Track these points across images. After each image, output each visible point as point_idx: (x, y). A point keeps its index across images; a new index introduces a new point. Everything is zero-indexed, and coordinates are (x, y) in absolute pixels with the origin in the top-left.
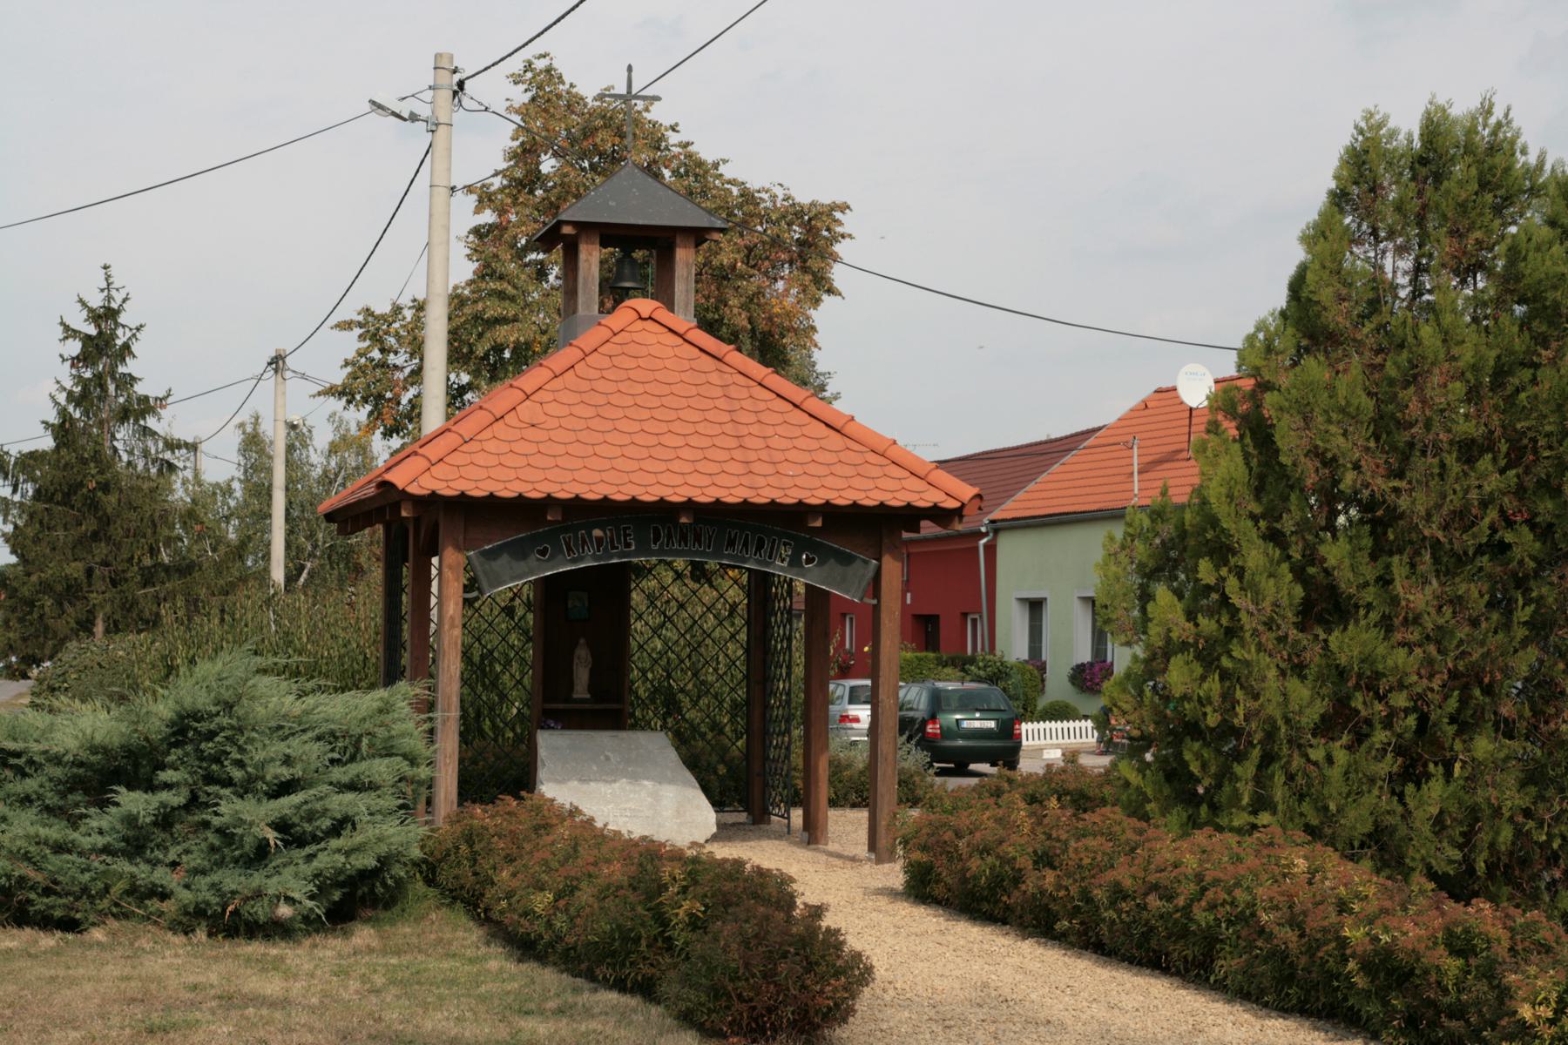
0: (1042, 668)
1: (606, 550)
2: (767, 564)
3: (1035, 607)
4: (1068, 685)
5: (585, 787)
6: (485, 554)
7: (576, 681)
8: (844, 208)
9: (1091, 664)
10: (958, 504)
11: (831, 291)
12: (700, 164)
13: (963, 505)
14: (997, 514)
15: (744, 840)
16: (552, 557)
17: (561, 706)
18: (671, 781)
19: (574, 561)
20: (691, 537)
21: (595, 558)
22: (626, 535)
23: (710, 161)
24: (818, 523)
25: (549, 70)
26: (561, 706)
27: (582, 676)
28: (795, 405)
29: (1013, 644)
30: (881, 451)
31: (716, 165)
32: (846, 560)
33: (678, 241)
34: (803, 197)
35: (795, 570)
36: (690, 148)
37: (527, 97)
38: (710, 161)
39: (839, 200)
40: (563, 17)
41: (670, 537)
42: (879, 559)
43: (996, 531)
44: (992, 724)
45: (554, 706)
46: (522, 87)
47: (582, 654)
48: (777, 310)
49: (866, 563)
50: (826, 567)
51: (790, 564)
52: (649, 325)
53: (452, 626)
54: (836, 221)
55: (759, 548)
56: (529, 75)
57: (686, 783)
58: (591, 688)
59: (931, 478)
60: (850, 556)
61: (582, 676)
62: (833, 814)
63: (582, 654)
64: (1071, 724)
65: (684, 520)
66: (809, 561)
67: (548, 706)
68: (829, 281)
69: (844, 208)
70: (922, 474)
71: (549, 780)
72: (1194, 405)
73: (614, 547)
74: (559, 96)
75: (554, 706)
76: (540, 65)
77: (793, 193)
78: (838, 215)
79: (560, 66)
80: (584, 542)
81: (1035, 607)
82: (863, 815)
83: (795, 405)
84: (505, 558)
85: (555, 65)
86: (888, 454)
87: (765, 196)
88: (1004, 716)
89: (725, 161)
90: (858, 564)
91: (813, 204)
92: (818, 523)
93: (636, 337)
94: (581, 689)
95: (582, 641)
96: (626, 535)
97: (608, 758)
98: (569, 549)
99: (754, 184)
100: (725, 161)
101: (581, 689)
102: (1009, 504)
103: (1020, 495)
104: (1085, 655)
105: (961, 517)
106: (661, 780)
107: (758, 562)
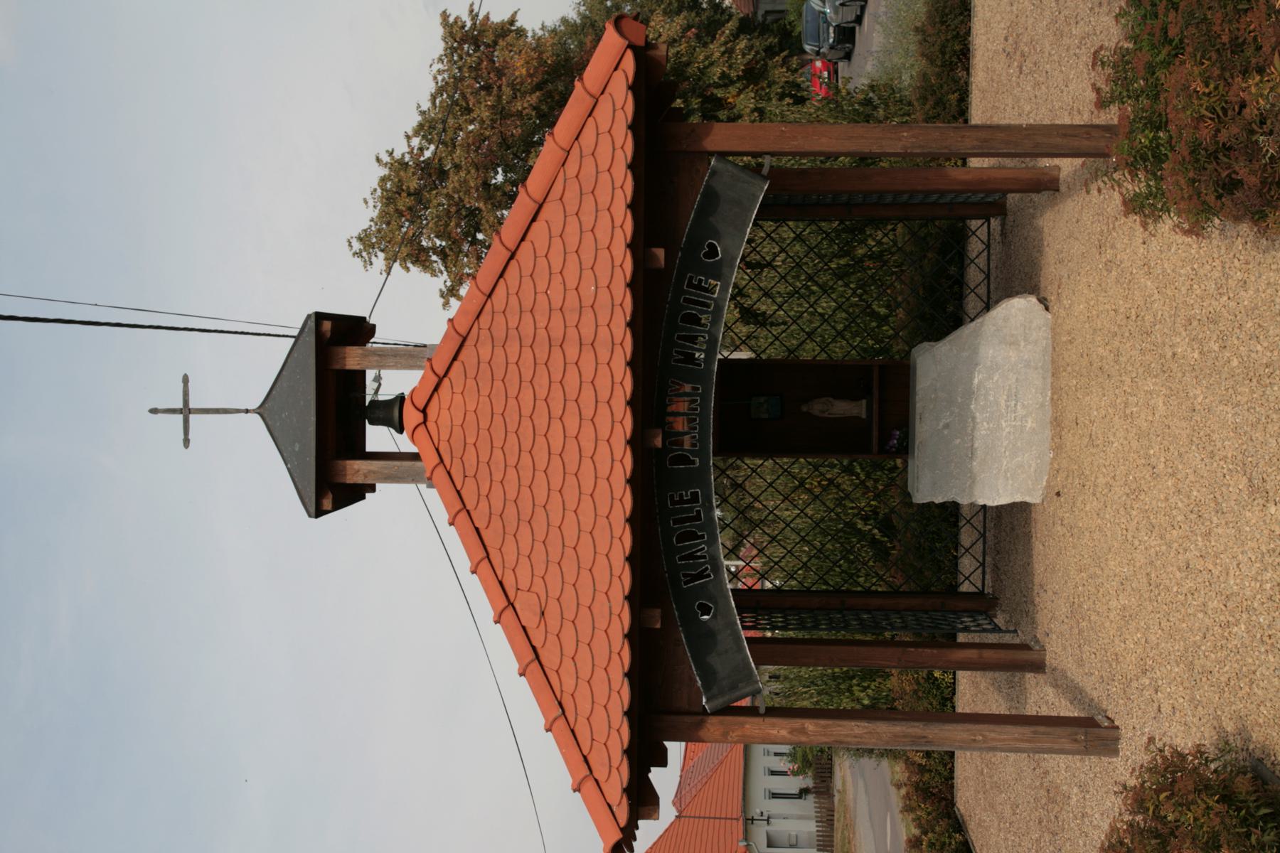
1: (701, 528)
5: (979, 453)
6: (707, 686)
8: (445, 16)
10: (629, 54)
11: (512, 21)
12: (421, 126)
13: (629, 46)
15: (1040, 252)
17: (875, 433)
18: (975, 350)
22: (682, 501)
23: (420, 118)
24: (660, 253)
25: (360, 239)
26: (875, 433)
27: (842, 408)
28: (512, 258)
30: (562, 154)
31: (423, 113)
32: (711, 198)
33: (338, 367)
34: (439, 47)
36: (410, 133)
37: (381, 255)
38: (420, 118)
39: (439, 20)
40: (236, 333)
42: (712, 154)
45: (875, 441)
46: (374, 259)
47: (817, 408)
48: (524, 71)
49: (714, 173)
51: (717, 278)
52: (432, 412)
53: (803, 731)
54: (456, 22)
56: (364, 254)
58: (855, 398)
59: (595, 90)
60: (704, 195)
61: (842, 408)
62: (978, 114)
63: (817, 408)
65: (658, 442)
66: (713, 252)
67: (875, 448)
68: (503, 24)
69: (445, 16)
70: (590, 101)
73: (698, 517)
74: (379, 231)
75: (875, 441)
76: (357, 246)
77: (437, 56)
78: (451, 20)
79: (356, 232)
80: (692, 556)
83: (512, 258)
84: (714, 660)
85: (356, 234)
86: (566, 146)
87: (440, 78)
89: (419, 106)
91: (444, 39)
93: (444, 437)
94: (858, 409)
95: (804, 409)
96: (682, 501)
97: (947, 426)
98: (701, 576)
99: (431, 87)
100: (419, 106)
101: (858, 409)
105: (649, 46)
106: (973, 364)
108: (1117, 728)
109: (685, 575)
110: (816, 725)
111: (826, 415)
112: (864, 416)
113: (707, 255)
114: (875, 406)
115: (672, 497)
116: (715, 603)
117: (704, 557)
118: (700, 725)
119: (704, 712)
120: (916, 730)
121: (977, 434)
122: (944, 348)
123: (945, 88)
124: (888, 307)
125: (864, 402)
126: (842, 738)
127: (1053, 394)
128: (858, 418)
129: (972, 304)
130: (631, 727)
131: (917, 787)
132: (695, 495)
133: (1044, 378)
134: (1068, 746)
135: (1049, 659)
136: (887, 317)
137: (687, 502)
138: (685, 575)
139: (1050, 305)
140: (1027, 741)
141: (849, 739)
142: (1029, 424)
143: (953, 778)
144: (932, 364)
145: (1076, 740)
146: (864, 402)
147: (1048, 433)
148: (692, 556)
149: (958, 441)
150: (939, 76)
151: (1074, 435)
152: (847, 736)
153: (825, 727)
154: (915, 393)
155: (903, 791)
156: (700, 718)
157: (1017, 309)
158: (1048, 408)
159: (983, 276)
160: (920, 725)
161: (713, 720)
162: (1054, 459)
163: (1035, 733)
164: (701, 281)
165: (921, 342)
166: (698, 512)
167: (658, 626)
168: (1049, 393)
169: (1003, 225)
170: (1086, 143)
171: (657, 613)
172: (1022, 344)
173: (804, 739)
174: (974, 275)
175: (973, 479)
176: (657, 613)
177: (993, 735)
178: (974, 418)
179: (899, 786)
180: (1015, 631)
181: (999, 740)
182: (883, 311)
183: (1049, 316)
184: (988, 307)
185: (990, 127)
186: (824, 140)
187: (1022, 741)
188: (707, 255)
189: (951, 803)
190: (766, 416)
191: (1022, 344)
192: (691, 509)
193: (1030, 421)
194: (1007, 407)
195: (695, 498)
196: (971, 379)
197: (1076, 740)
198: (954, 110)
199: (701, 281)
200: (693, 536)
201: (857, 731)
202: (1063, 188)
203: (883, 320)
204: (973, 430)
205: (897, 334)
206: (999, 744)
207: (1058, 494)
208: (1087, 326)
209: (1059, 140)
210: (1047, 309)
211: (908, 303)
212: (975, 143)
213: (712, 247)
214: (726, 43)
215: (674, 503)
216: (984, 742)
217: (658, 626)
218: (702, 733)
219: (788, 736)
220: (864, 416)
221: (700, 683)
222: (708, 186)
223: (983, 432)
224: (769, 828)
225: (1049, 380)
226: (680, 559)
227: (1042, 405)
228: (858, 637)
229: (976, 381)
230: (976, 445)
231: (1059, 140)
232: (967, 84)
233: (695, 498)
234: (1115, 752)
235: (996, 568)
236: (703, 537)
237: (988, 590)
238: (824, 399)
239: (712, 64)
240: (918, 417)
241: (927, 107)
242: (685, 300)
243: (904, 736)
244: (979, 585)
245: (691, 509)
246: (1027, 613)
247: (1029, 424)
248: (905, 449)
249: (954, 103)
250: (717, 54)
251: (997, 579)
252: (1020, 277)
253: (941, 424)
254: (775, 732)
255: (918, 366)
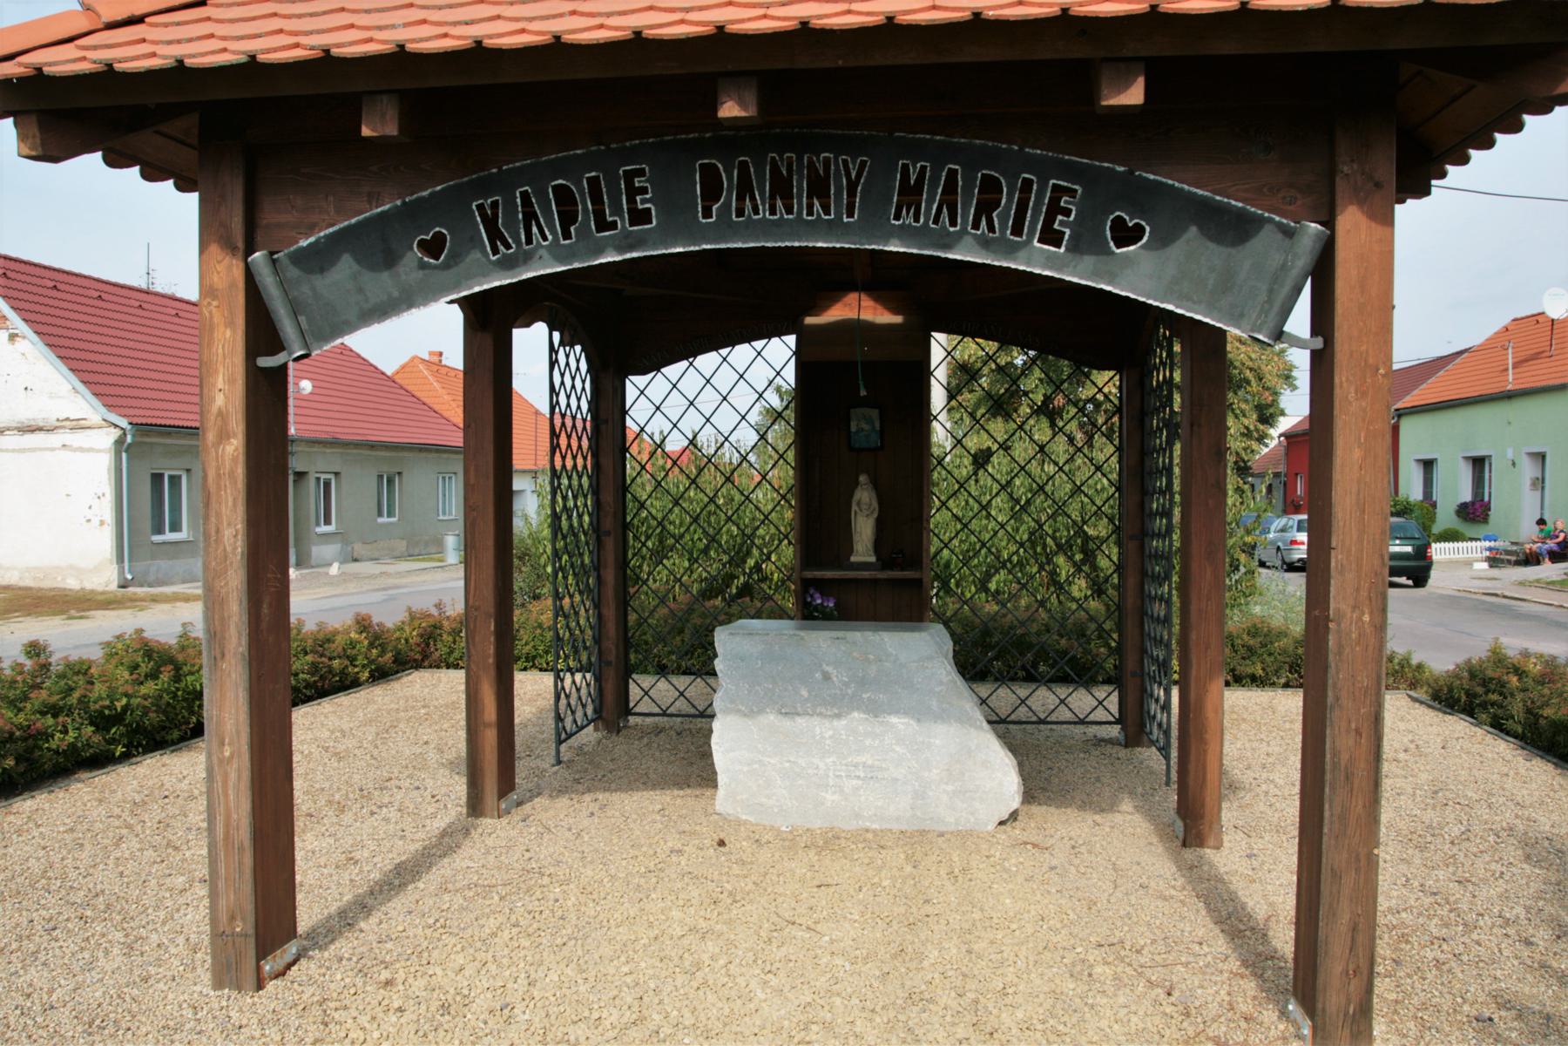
0: (1434, 505)
1: (584, 232)
2: (1011, 250)
3: (1428, 465)
4: (1454, 517)
5: (787, 724)
7: (856, 538)
9: (1473, 503)
14: (1399, 405)
16: (455, 258)
18: (941, 717)
19: (508, 264)
20: (800, 186)
21: (559, 254)
22: (633, 192)
24: (1134, 95)
26: (829, 574)
27: (864, 530)
29: (1412, 487)
32: (1233, 228)
35: (1088, 261)
41: (745, 189)
42: (1329, 223)
43: (1399, 416)
44: (1409, 549)
45: (818, 574)
47: (864, 496)
49: (1289, 233)
50: (1177, 250)
53: (224, 436)
55: (986, 208)
57: (964, 720)
60: (1241, 216)
61: (864, 530)
63: (864, 496)
64: (1460, 545)
65: (730, 110)
67: (809, 574)
71: (727, 711)
72: (1555, 317)
73: (603, 225)
75: (818, 574)
80: (530, 216)
81: (1428, 465)
82: (1289, 704)
84: (346, 266)
88: (1418, 543)
90: (1265, 243)
92: (1134, 95)
95: (863, 478)
96: (633, 192)
97: (827, 677)
98: (495, 235)
102: (1408, 398)
103: (1416, 392)
104: (1467, 497)
106: (921, 713)
107: (985, 244)
108: (260, 986)
109: (495, 205)
110: (234, 459)
111: (854, 507)
112: (853, 559)
113: (1118, 224)
114: (866, 574)
115: (641, 173)
116: (446, 266)
117: (529, 241)
118: (230, 247)
119: (249, 251)
120: (234, 640)
121: (816, 721)
122: (944, 672)
123: (1269, 660)
124: (997, 592)
125: (873, 559)
126: (214, 505)
127: (874, 831)
128: (851, 551)
129: (1004, 697)
130: (151, 74)
131: (437, 626)
132: (644, 217)
133: (898, 819)
134: (223, 903)
135: (487, 822)
136: (987, 590)
137: (631, 201)
138: (495, 205)
139: (1007, 828)
140: (227, 834)
141: (213, 519)
142: (830, 797)
143: (448, 667)
144: (923, 652)
145: (232, 918)
146: (873, 559)
147: (817, 824)
148: (530, 216)
149: (805, 693)
150: (1284, 652)
151: (802, 880)
152: (219, 515)
153: (232, 473)
154: (876, 630)
155: (435, 612)
156: (241, 244)
157: (997, 775)
158: (852, 825)
159: (1042, 716)
160: (243, 649)
161: (241, 265)
162: (779, 832)
163: (241, 849)
164: (1067, 213)
165: (953, 635)
166: (613, 226)
167: (366, 132)
168: (875, 826)
169: (1111, 742)
170: (1338, 968)
171: (392, 130)
172: (950, 788)
173: (211, 436)
174: (1043, 699)
175: (750, 714)
176: (392, 130)
177: (233, 776)
178: (838, 716)
179: (438, 606)
180: (559, 762)
181: (225, 783)
182: (992, 586)
183: (991, 827)
184: (998, 723)
185: (1376, 784)
186: (1357, 454)
187: (227, 826)
188: (1118, 224)
189: (418, 665)
190: (853, 428)
191: (950, 788)
192: (617, 210)
193: (836, 797)
194: (856, 766)
195: (640, 217)
196: (897, 712)
197: (232, 918)
198: (1240, 670)
199: (1067, 213)
200: (568, 219)
201: (228, 533)
202: (1189, 854)
203: (983, 586)
204: (820, 714)
205: (965, 603)
206: (218, 785)
207: (722, 843)
208: (977, 915)
209: (1344, 918)
210: (1001, 823)
211: (1005, 616)
212: (1345, 757)
213: (1137, 234)
214: (1257, 430)
215: (629, 176)
216: (221, 761)
217: (366, 132)
218: (214, 249)
219: (214, 410)
220: (853, 559)
221: (304, 243)
222: (1260, 222)
223: (818, 730)
224: (528, 493)
225: (896, 827)
226: (525, 195)
227: (857, 816)
228: (1176, 629)
229: (894, 720)
230: (799, 720)
231: (1344, 918)
232: (1273, 684)
233: (640, 217)
234: (218, 984)
235: (658, 731)
236: (567, 235)
237: (632, 720)
238: (875, 504)
239: (1236, 417)
240: (840, 634)
241: (1245, 636)
242: (1027, 184)
243: (222, 619)
244: (637, 710)
245: (617, 210)
246: (577, 781)
247: (830, 797)
248: (809, 614)
249: (1250, 670)
250: (1246, 422)
251: (644, 732)
252: (1046, 774)
253: (829, 669)
254: (220, 384)
255: (916, 635)
